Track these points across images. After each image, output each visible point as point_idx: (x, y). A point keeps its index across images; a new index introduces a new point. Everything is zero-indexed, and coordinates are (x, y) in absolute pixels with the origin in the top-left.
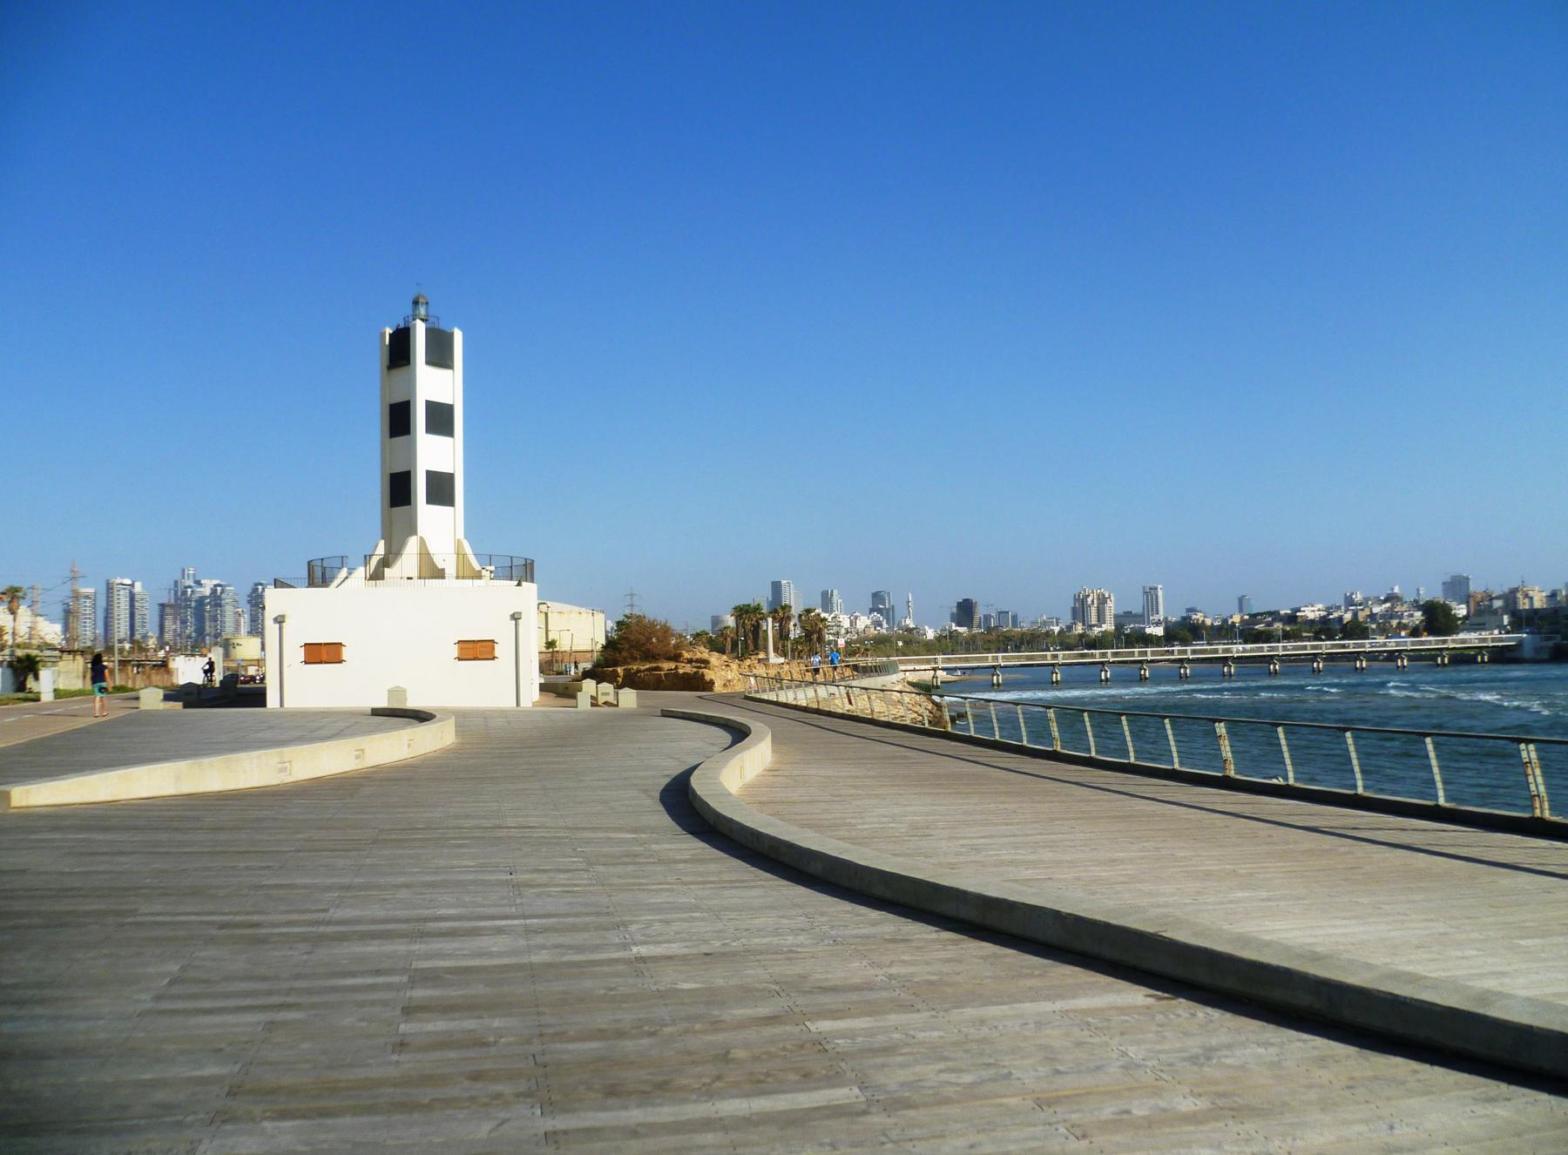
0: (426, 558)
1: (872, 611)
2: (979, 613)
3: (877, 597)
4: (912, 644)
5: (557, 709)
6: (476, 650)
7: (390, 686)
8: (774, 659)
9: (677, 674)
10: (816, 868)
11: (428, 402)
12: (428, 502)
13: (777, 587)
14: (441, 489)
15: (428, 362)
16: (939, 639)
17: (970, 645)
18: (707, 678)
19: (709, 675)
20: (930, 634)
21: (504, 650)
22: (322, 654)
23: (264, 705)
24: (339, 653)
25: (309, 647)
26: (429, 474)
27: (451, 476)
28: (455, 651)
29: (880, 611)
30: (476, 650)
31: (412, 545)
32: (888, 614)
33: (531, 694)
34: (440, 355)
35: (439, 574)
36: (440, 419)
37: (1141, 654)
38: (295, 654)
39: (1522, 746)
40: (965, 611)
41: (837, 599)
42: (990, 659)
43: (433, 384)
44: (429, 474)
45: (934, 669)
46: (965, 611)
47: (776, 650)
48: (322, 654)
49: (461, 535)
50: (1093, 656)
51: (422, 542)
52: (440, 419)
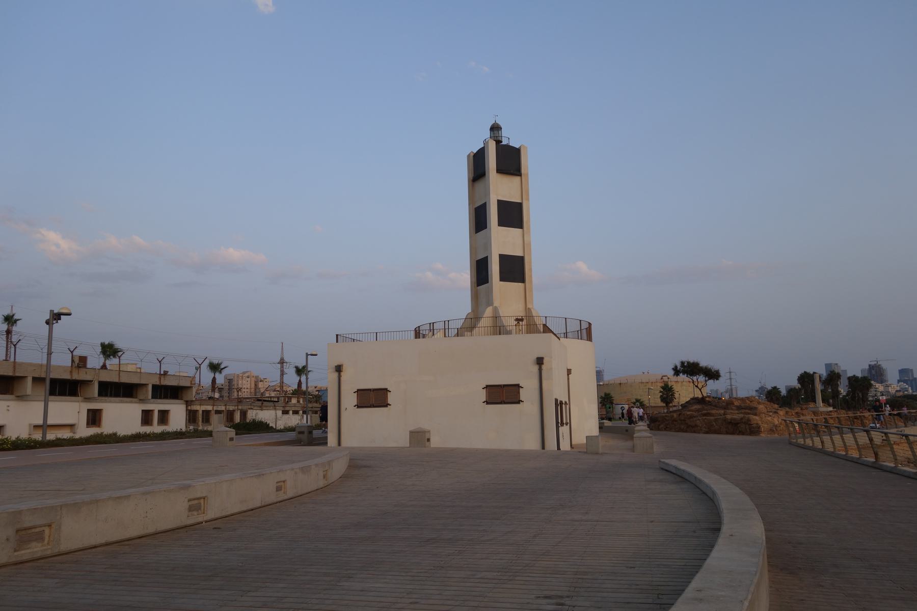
0: (496, 317)
5: (613, 445)
6: (503, 394)
8: (822, 407)
9: (725, 420)
10: (117, 395)
11: (499, 202)
12: (501, 280)
15: (500, 171)
19: (755, 419)
21: (529, 393)
22: (372, 398)
24: (489, 395)
25: (360, 392)
26: (502, 257)
28: (483, 396)
30: (503, 394)
31: (489, 312)
38: (349, 400)
39: (855, 454)
44: (502, 257)
47: (823, 401)
51: (496, 310)
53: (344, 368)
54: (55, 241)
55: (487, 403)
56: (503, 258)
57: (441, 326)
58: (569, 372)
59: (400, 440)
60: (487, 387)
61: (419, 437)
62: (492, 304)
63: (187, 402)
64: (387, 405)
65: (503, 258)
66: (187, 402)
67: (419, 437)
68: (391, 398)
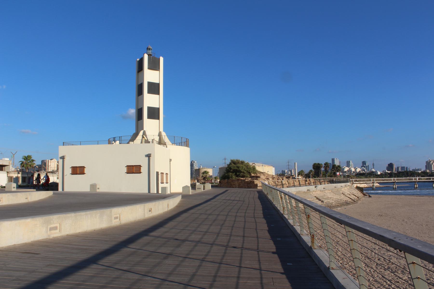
1: (362, 167)
2: (395, 167)
3: (364, 163)
4: (372, 175)
6: (133, 169)
7: (91, 183)
13: (333, 160)
14: (154, 113)
16: (381, 174)
17: (391, 175)
18: (255, 183)
20: (379, 173)
21: (144, 170)
22: (78, 171)
23: (57, 190)
24: (83, 170)
27: (158, 109)
28: (125, 170)
29: (364, 167)
30: (133, 169)
31: (141, 133)
32: (367, 167)
33: (210, 188)
34: (154, 66)
35: (149, 142)
36: (154, 88)
37: (415, 179)
40: (390, 166)
41: (351, 163)
42: (392, 179)
43: (150, 76)
45: (373, 183)
46: (390, 166)
48: (78, 171)
49: (162, 130)
50: (412, 179)
52: (154, 88)
53: (152, 155)
54: (5, 87)
55: (127, 173)
56: (149, 109)
57: (112, 139)
58: (171, 160)
59: (86, 189)
60: (127, 166)
61: (93, 186)
62: (143, 129)
63: (8, 172)
64: (84, 174)
65: (149, 109)
66: (8, 172)
67: (93, 186)
68: (86, 171)
